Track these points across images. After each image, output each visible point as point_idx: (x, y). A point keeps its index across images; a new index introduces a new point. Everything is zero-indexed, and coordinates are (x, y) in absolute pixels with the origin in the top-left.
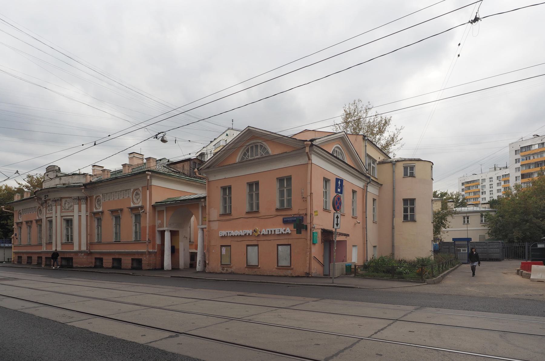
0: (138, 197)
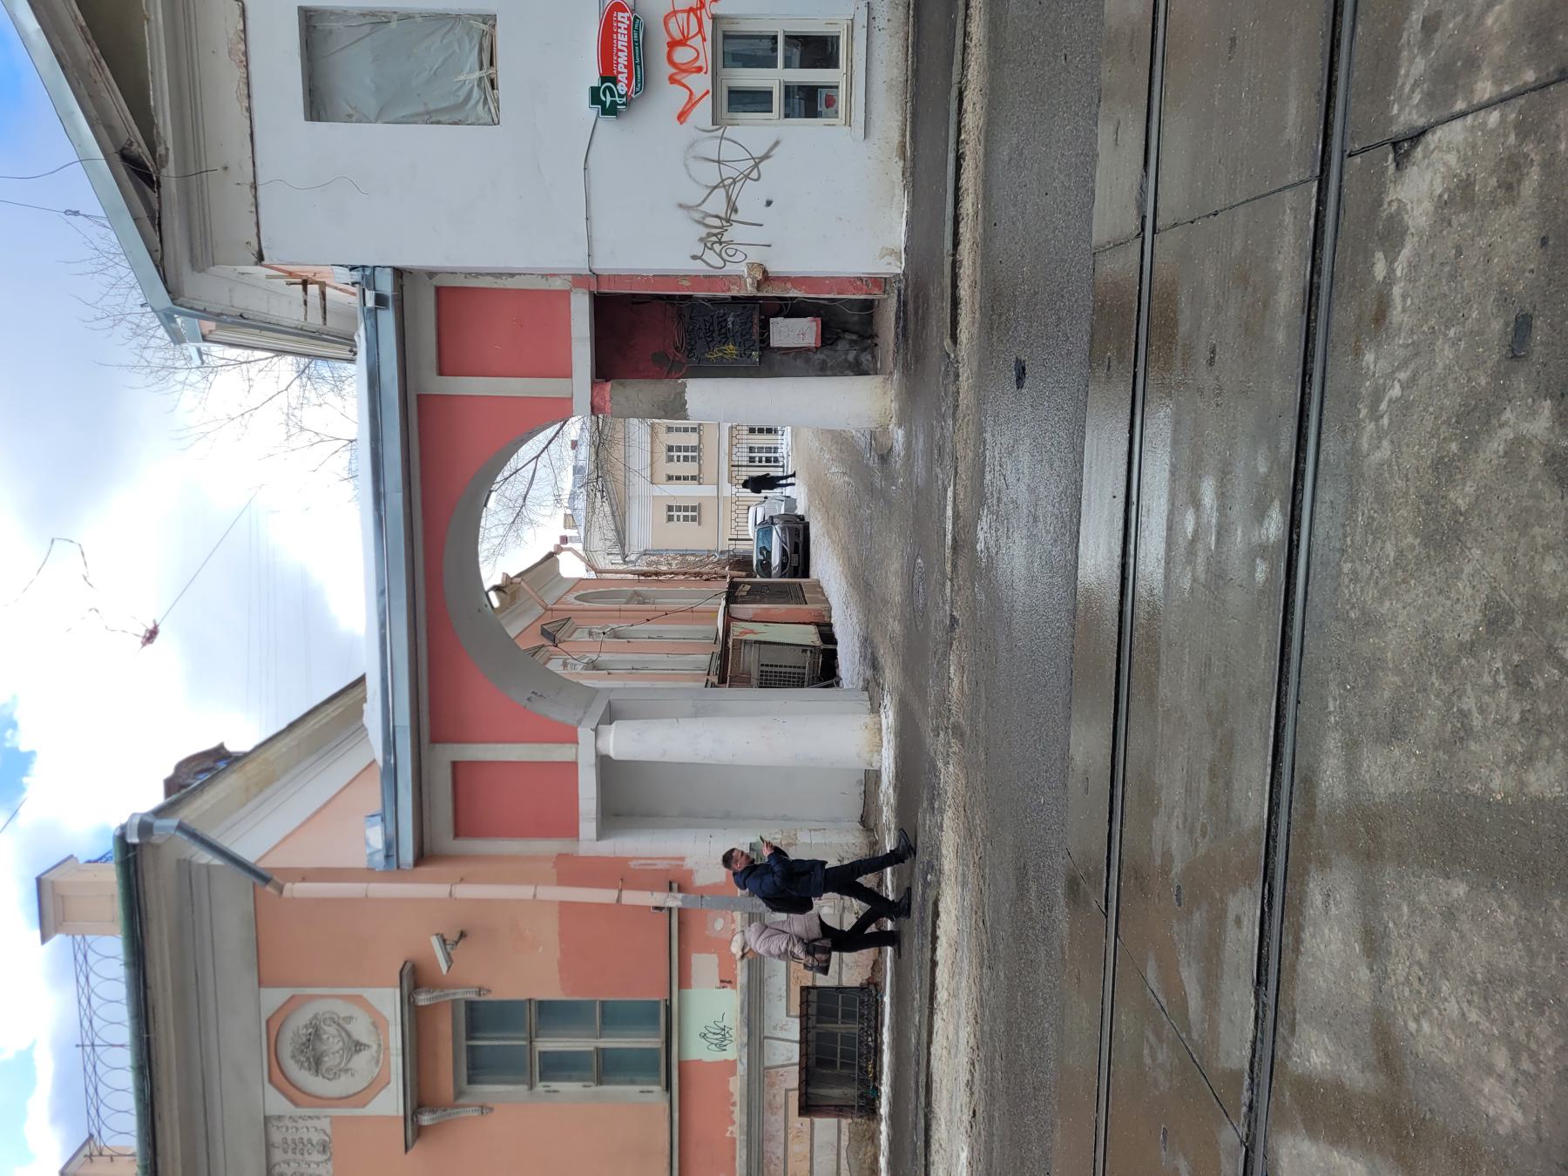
0: (332, 1042)
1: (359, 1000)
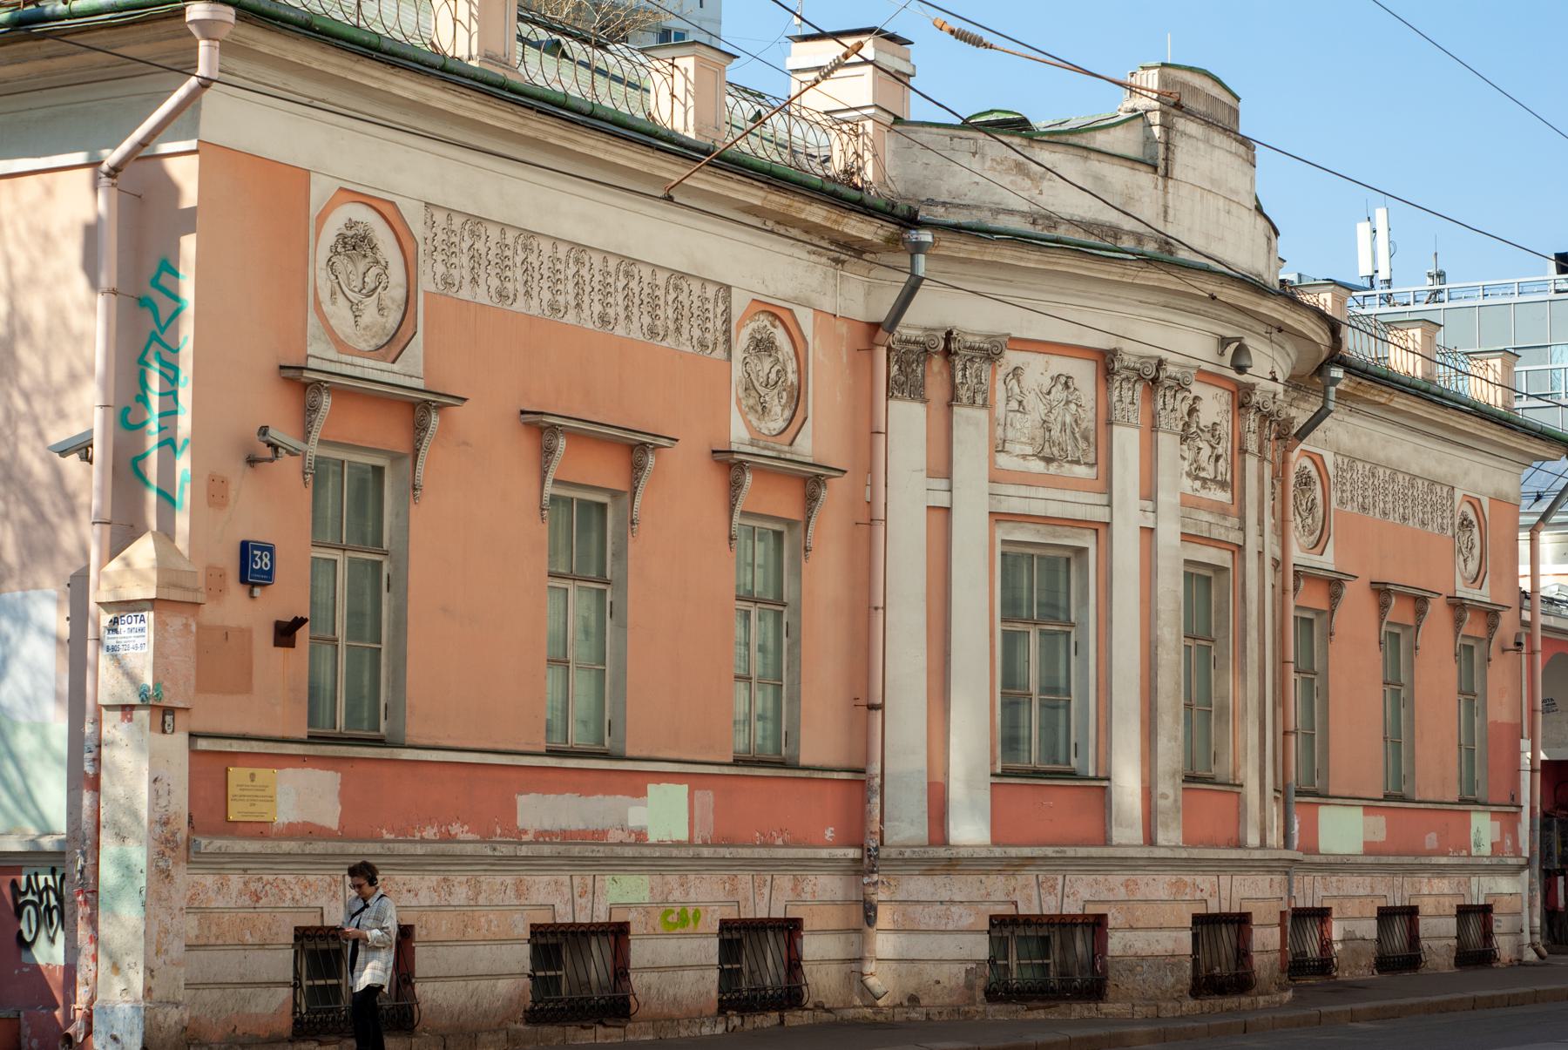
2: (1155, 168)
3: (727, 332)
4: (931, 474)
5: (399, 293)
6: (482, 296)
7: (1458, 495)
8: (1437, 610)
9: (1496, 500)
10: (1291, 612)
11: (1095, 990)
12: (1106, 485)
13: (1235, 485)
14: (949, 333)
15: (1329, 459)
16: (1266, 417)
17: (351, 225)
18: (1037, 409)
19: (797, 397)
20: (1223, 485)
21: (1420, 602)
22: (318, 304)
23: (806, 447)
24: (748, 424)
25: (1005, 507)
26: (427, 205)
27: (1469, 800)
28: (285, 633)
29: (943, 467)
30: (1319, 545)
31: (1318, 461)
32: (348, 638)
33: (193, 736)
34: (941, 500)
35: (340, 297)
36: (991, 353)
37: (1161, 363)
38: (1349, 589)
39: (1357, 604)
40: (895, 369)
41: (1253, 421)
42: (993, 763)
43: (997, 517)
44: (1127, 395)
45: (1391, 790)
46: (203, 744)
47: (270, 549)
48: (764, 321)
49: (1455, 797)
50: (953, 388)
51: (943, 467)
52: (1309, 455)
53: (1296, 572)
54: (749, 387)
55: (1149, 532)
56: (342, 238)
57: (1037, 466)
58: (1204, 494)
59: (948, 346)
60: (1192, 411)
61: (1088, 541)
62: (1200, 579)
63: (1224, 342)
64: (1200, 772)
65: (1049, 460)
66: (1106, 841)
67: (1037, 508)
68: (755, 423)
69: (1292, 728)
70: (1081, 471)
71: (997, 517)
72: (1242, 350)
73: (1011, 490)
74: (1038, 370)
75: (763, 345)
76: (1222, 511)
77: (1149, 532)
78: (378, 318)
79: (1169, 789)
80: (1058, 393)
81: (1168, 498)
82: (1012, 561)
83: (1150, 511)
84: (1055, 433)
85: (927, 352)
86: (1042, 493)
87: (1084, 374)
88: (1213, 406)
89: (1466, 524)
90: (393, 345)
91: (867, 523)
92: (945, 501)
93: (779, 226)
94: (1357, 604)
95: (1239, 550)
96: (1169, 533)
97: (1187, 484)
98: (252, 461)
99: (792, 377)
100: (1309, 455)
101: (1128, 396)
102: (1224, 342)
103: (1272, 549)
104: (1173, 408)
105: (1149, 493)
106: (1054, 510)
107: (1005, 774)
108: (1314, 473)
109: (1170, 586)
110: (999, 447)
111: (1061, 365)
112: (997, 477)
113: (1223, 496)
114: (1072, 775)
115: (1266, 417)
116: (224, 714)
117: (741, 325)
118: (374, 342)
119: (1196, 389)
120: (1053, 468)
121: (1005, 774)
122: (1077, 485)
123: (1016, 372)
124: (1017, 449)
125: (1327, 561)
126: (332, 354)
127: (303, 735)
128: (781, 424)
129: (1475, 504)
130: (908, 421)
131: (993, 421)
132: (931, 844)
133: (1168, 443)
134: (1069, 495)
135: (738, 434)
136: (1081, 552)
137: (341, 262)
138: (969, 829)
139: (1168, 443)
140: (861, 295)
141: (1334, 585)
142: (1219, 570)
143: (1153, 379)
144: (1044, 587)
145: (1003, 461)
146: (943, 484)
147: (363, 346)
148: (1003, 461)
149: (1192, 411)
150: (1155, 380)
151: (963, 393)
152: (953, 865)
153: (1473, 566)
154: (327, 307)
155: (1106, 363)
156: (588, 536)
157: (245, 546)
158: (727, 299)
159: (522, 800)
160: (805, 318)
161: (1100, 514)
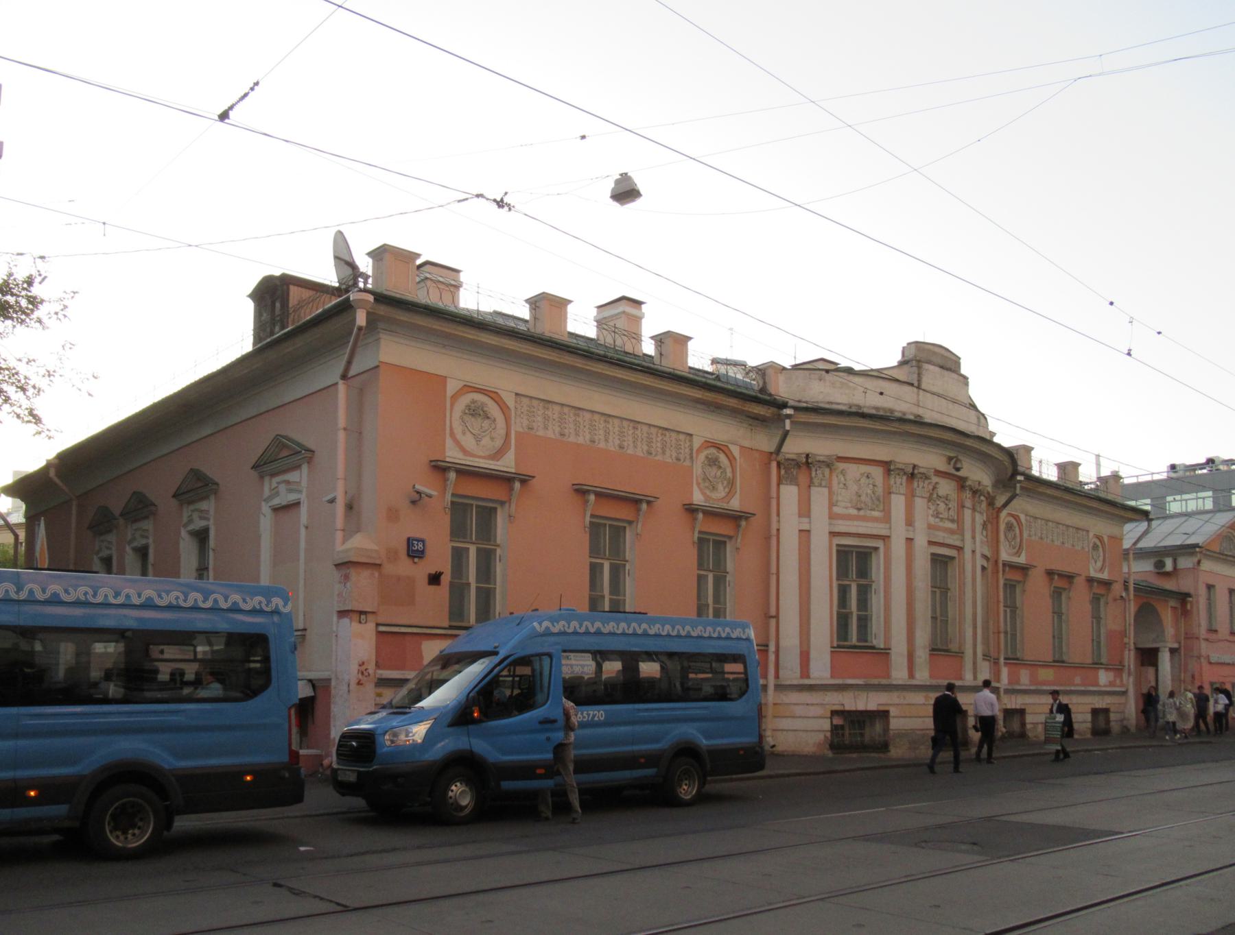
1: (455, 397)
2: (912, 385)
3: (691, 454)
4: (800, 516)
5: (503, 432)
6: (550, 434)
7: (1091, 535)
8: (1080, 582)
9: (1111, 537)
10: (1002, 582)
11: (884, 747)
12: (887, 518)
13: (959, 521)
14: (807, 456)
15: (1022, 517)
16: (975, 492)
17: (474, 402)
18: (854, 488)
19: (731, 483)
20: (952, 521)
21: (1069, 578)
22: (452, 434)
23: (735, 504)
24: (704, 494)
25: (836, 530)
26: (517, 394)
27: (1097, 665)
28: (435, 579)
29: (805, 510)
30: (1018, 553)
31: (1016, 518)
32: (477, 581)
33: (378, 625)
34: (806, 527)
35: (468, 434)
36: (828, 464)
37: (914, 467)
38: (1032, 573)
39: (1037, 580)
40: (783, 472)
41: (968, 494)
42: (832, 642)
43: (833, 534)
44: (898, 481)
45: (1057, 658)
46: (382, 629)
47: (423, 541)
48: (713, 451)
49: (1090, 661)
50: (811, 478)
51: (805, 510)
52: (1010, 515)
53: (1004, 565)
54: (705, 479)
55: (910, 540)
56: (468, 407)
57: (854, 512)
58: (941, 524)
59: (807, 463)
60: (934, 488)
61: (880, 544)
62: (940, 563)
63: (950, 459)
64: (940, 646)
65: (859, 509)
66: (888, 676)
67: (853, 530)
68: (708, 492)
69: (1002, 628)
70: (876, 514)
71: (833, 534)
72: (958, 460)
73: (840, 522)
74: (854, 470)
75: (713, 462)
76: (952, 532)
77: (910, 540)
78: (490, 443)
79: (922, 655)
80: (863, 480)
81: (920, 524)
82: (843, 554)
83: (908, 531)
84: (863, 498)
85: (798, 465)
86: (855, 523)
87: (877, 472)
88: (946, 487)
89: (1095, 547)
90: (499, 454)
91: (769, 539)
92: (807, 529)
93: (716, 408)
94: (1037, 580)
95: (960, 549)
96: (921, 541)
97: (932, 520)
98: (414, 502)
99: (729, 474)
100: (1010, 515)
101: (899, 482)
102: (950, 459)
103: (983, 549)
104: (921, 488)
105: (910, 522)
106: (861, 531)
107: (839, 647)
108: (1015, 524)
109: (922, 565)
110: (832, 504)
111: (864, 468)
112: (832, 516)
113: (954, 526)
114: (873, 647)
115: (975, 492)
116: (403, 617)
117: (698, 451)
118: (487, 453)
119: (935, 479)
120: (862, 513)
121: (839, 647)
122: (875, 520)
123: (843, 472)
124: (843, 504)
125: (1022, 560)
126: (461, 455)
127: (446, 624)
128: (723, 494)
129: (1099, 538)
130: (790, 494)
131: (831, 493)
132: (802, 677)
133: (920, 503)
134: (869, 524)
135: (698, 498)
136: (876, 549)
137: (467, 418)
138: (821, 670)
139: (920, 503)
140: (764, 441)
141: (1024, 569)
142: (952, 558)
143: (912, 475)
144: (855, 562)
145: (836, 509)
146: (806, 520)
147: (481, 454)
148: (836, 509)
149: (934, 488)
150: (912, 474)
151: (816, 481)
152: (811, 688)
153: (1099, 564)
154: (459, 436)
155: (887, 466)
156: (607, 539)
157: (409, 539)
158: (691, 441)
159: (658, 676)
160: (735, 451)
161: (883, 532)
